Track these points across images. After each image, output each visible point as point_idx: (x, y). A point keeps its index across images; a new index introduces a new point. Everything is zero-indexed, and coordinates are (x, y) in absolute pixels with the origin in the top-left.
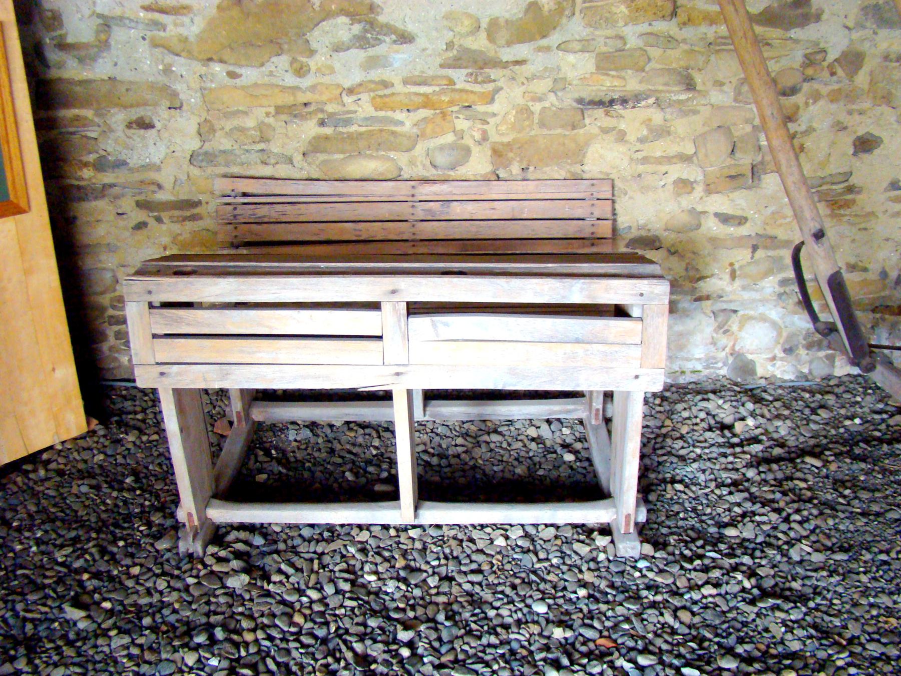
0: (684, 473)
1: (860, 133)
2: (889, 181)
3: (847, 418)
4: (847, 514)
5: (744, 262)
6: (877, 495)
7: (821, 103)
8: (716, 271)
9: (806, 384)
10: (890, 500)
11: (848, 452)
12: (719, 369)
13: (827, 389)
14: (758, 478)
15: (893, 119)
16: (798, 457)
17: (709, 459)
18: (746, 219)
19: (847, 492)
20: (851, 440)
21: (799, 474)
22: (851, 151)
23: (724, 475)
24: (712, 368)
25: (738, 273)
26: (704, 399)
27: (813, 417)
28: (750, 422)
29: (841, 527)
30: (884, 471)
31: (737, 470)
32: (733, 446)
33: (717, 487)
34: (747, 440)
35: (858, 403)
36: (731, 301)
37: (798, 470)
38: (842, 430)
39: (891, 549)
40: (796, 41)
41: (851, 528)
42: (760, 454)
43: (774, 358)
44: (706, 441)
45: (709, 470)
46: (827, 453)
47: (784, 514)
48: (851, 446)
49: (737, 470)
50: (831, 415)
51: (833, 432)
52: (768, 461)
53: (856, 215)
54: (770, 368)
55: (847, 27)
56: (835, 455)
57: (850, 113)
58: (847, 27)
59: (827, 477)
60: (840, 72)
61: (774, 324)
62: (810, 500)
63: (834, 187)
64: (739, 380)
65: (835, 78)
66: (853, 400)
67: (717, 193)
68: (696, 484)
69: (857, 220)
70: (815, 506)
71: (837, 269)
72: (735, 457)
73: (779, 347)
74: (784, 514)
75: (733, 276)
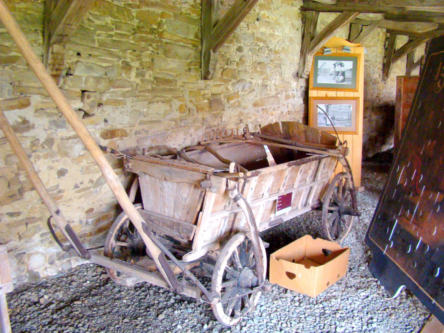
0: (26, 328)
1: (59, 169)
2: (74, 185)
3: (84, 282)
4: (98, 317)
5: (24, 231)
6: (106, 306)
7: (41, 160)
8: (13, 238)
9: (62, 275)
10: (112, 305)
11: (89, 294)
12: (24, 280)
13: (72, 274)
14: (59, 317)
15: (70, 162)
16: (71, 303)
17: (35, 318)
18: (20, 213)
19: (95, 309)
20: (90, 289)
21: (74, 309)
22: (57, 176)
23: (44, 321)
24: (21, 280)
25: (22, 236)
26: (22, 295)
27: (71, 286)
28: (46, 297)
29: (98, 322)
30: (106, 296)
31: (48, 317)
32: (43, 309)
33: (43, 327)
34: (48, 304)
35: (85, 275)
36: (22, 249)
37: (73, 308)
38: (84, 288)
39: (119, 322)
40: (27, 137)
41: (102, 321)
42: (55, 308)
43: (46, 268)
44: (30, 311)
45: (37, 322)
46: (81, 298)
47: (75, 326)
48: (90, 292)
49: (48, 317)
50: (77, 283)
51: (81, 289)
52: (60, 309)
53: (65, 201)
54: (45, 273)
55: (45, 130)
56: (85, 297)
57: (53, 162)
58: (45, 130)
59: (85, 306)
60: (46, 147)
61: (42, 254)
62: (82, 317)
63: (53, 192)
64: (34, 282)
65: (44, 149)
66: (83, 275)
67: (6, 204)
68: (33, 330)
69: (65, 203)
70: (85, 318)
71: (67, 223)
72: (46, 313)
73: (47, 263)
74: (75, 326)
75: (20, 238)
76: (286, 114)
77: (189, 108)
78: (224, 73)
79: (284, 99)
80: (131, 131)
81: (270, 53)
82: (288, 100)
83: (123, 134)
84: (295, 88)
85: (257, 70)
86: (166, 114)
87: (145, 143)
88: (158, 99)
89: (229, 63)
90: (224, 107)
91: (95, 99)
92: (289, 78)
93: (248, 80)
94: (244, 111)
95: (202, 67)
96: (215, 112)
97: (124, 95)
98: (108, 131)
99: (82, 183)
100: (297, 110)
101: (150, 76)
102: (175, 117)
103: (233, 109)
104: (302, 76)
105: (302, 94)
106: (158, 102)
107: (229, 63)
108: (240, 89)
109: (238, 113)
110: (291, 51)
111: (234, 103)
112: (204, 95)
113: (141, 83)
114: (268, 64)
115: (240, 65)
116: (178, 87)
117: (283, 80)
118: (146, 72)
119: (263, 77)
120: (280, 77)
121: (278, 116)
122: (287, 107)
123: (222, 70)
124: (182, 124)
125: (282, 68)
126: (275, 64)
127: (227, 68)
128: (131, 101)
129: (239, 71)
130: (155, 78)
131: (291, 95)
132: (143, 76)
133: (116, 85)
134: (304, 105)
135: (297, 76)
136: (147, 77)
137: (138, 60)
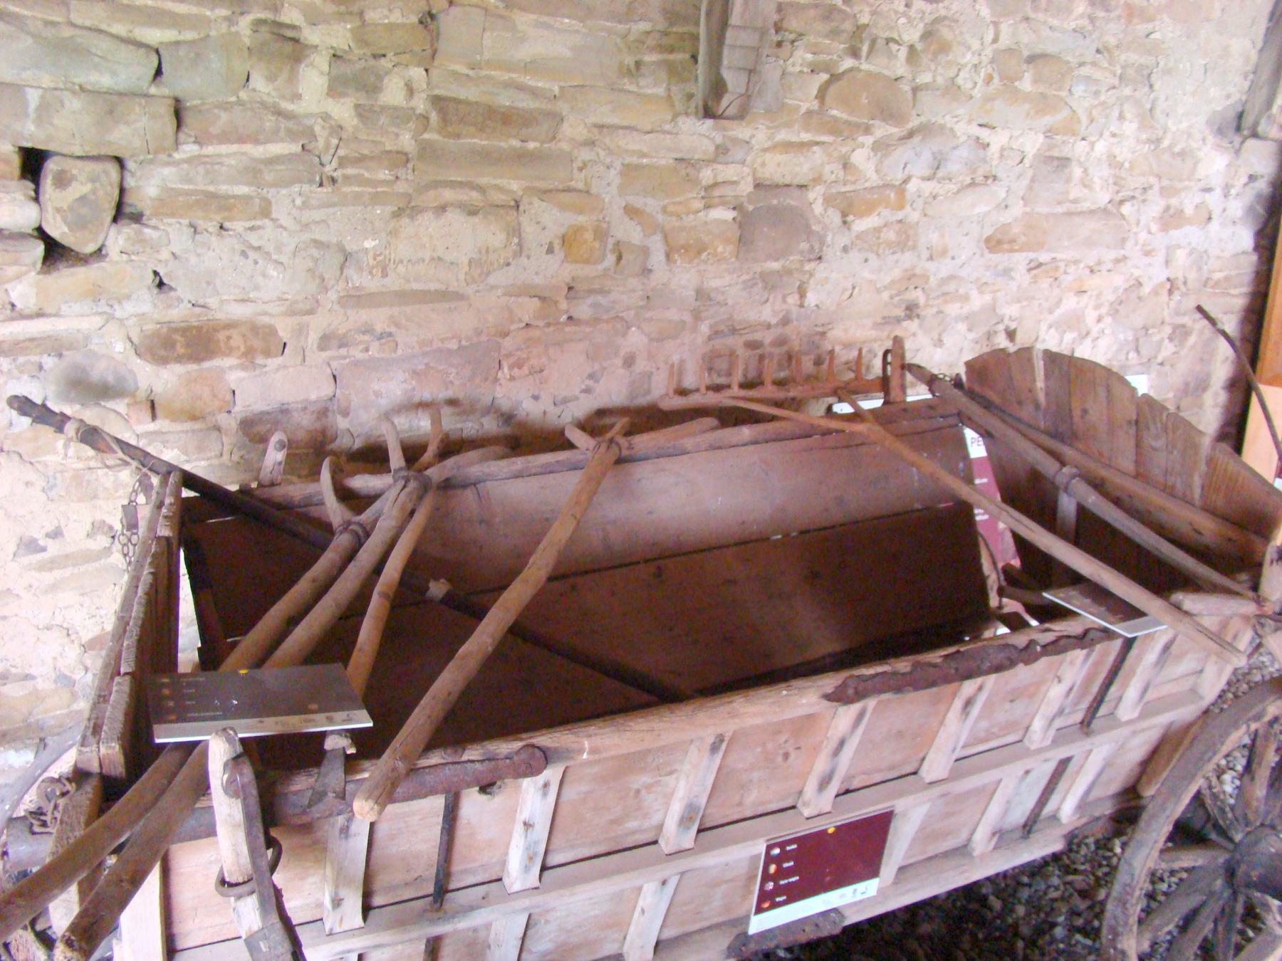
76: (1155, 292)
77: (618, 243)
78: (833, 89)
79: (1154, 228)
80: (301, 331)
81: (1101, 14)
82: (1175, 234)
83: (257, 343)
84: (1217, 182)
85: (1016, 91)
86: (481, 266)
87: (376, 386)
88: (448, 195)
89: (865, 48)
90: (822, 242)
91: (94, 192)
92: (1190, 135)
93: (966, 130)
94: (931, 266)
95: (701, 59)
96: (775, 266)
97: (253, 172)
98: (176, 330)
99: (56, 534)
100: (1218, 276)
101: (410, 91)
102: (538, 280)
103: (871, 256)
104: (1261, 129)
105: (1250, 210)
106: (442, 209)
107: (865, 48)
108: (920, 167)
109: (897, 273)
110: (1217, 14)
111: (877, 230)
112: (715, 185)
113: (356, 121)
114: (1081, 64)
115: (925, 59)
116: (565, 146)
117: (1158, 141)
118: (388, 73)
119: (1047, 120)
120: (1143, 126)
121: (1112, 298)
122: (1167, 263)
123: (825, 77)
124: (583, 310)
125: (1156, 87)
126: (1123, 68)
127: (851, 70)
128: (299, 202)
129: (915, 90)
130: (437, 101)
131: (1189, 210)
132: (374, 89)
133: (214, 130)
134: (1254, 258)
135: (1238, 129)
136: (393, 93)
137: (341, 17)
